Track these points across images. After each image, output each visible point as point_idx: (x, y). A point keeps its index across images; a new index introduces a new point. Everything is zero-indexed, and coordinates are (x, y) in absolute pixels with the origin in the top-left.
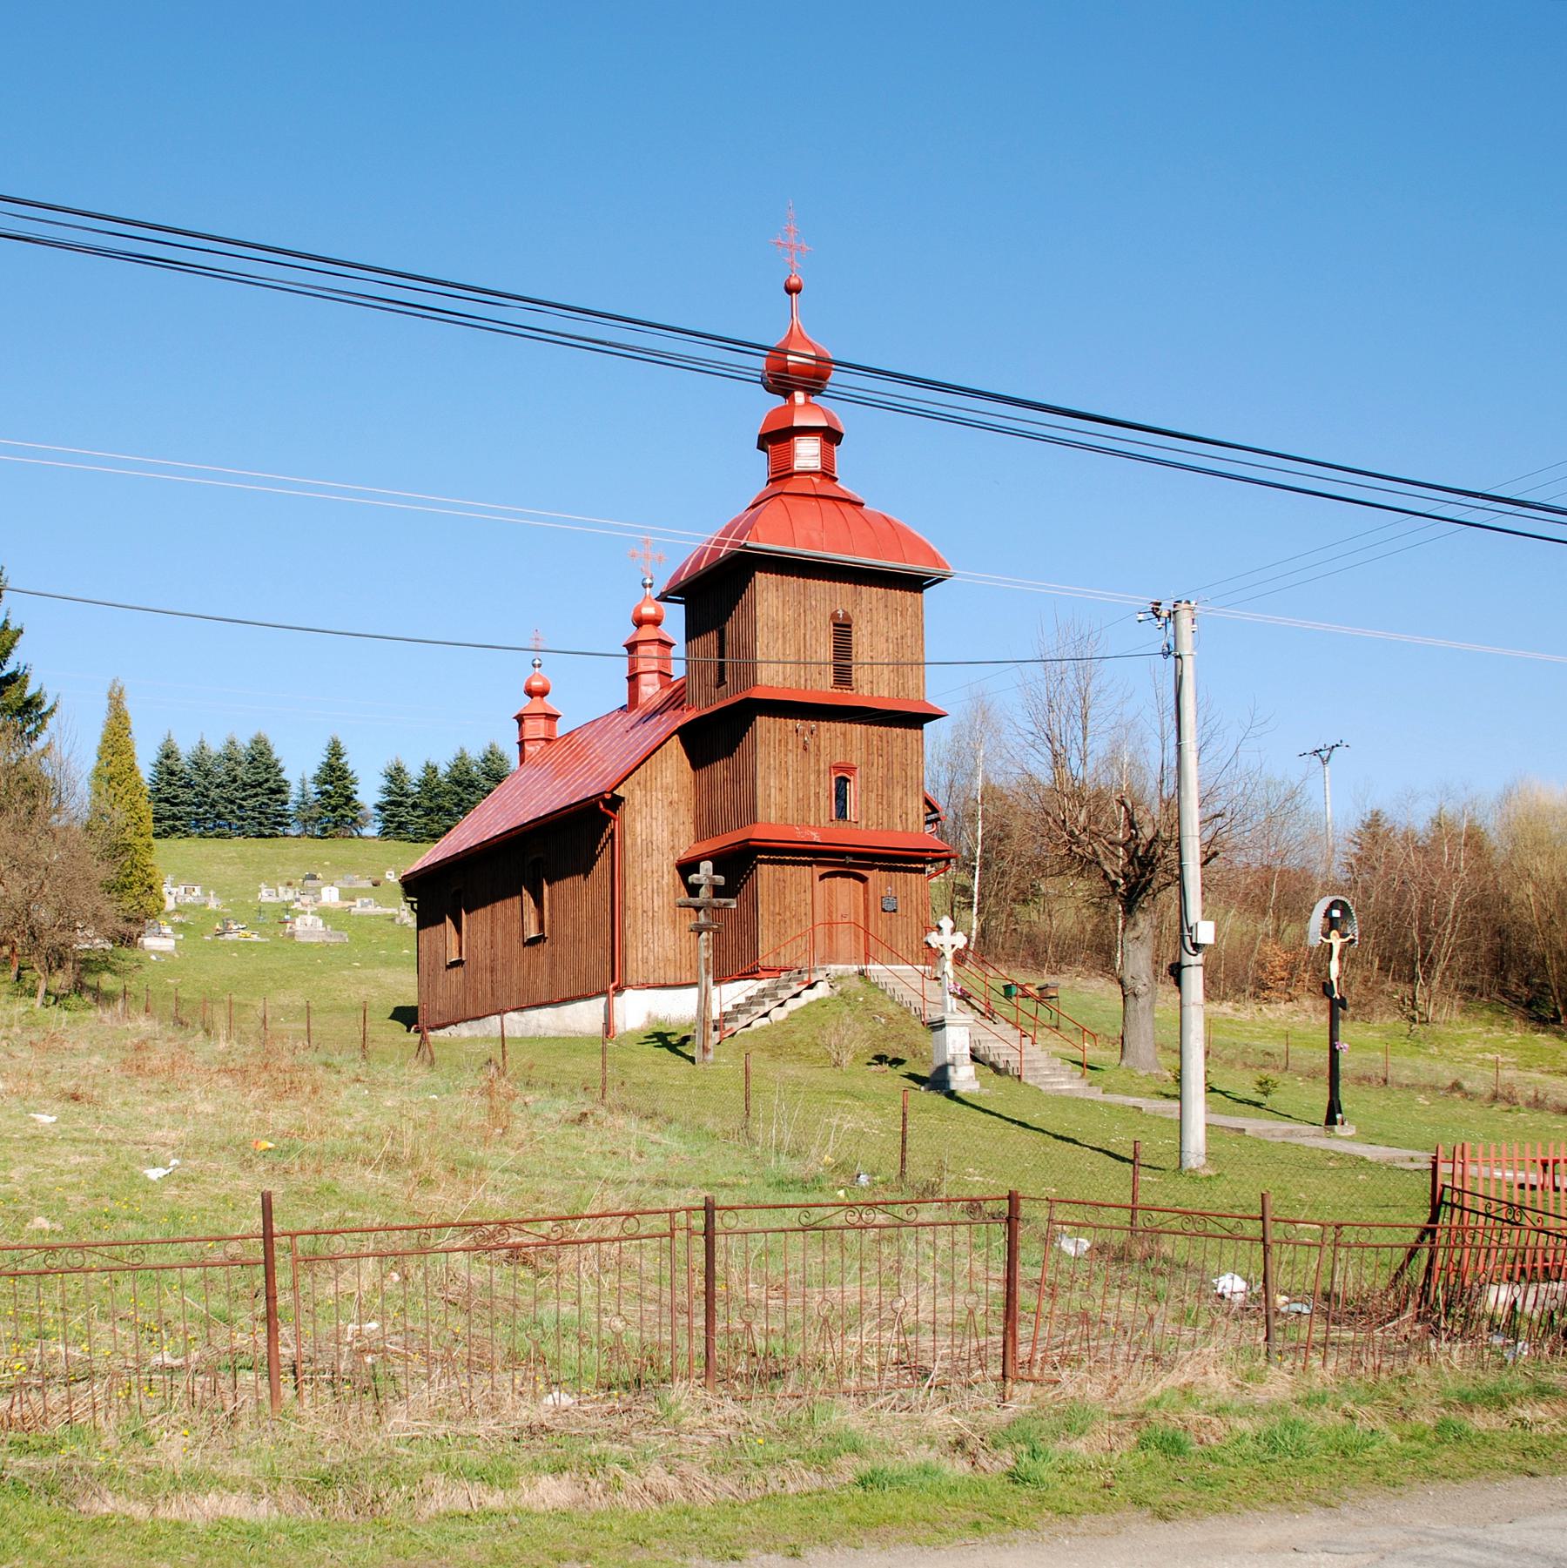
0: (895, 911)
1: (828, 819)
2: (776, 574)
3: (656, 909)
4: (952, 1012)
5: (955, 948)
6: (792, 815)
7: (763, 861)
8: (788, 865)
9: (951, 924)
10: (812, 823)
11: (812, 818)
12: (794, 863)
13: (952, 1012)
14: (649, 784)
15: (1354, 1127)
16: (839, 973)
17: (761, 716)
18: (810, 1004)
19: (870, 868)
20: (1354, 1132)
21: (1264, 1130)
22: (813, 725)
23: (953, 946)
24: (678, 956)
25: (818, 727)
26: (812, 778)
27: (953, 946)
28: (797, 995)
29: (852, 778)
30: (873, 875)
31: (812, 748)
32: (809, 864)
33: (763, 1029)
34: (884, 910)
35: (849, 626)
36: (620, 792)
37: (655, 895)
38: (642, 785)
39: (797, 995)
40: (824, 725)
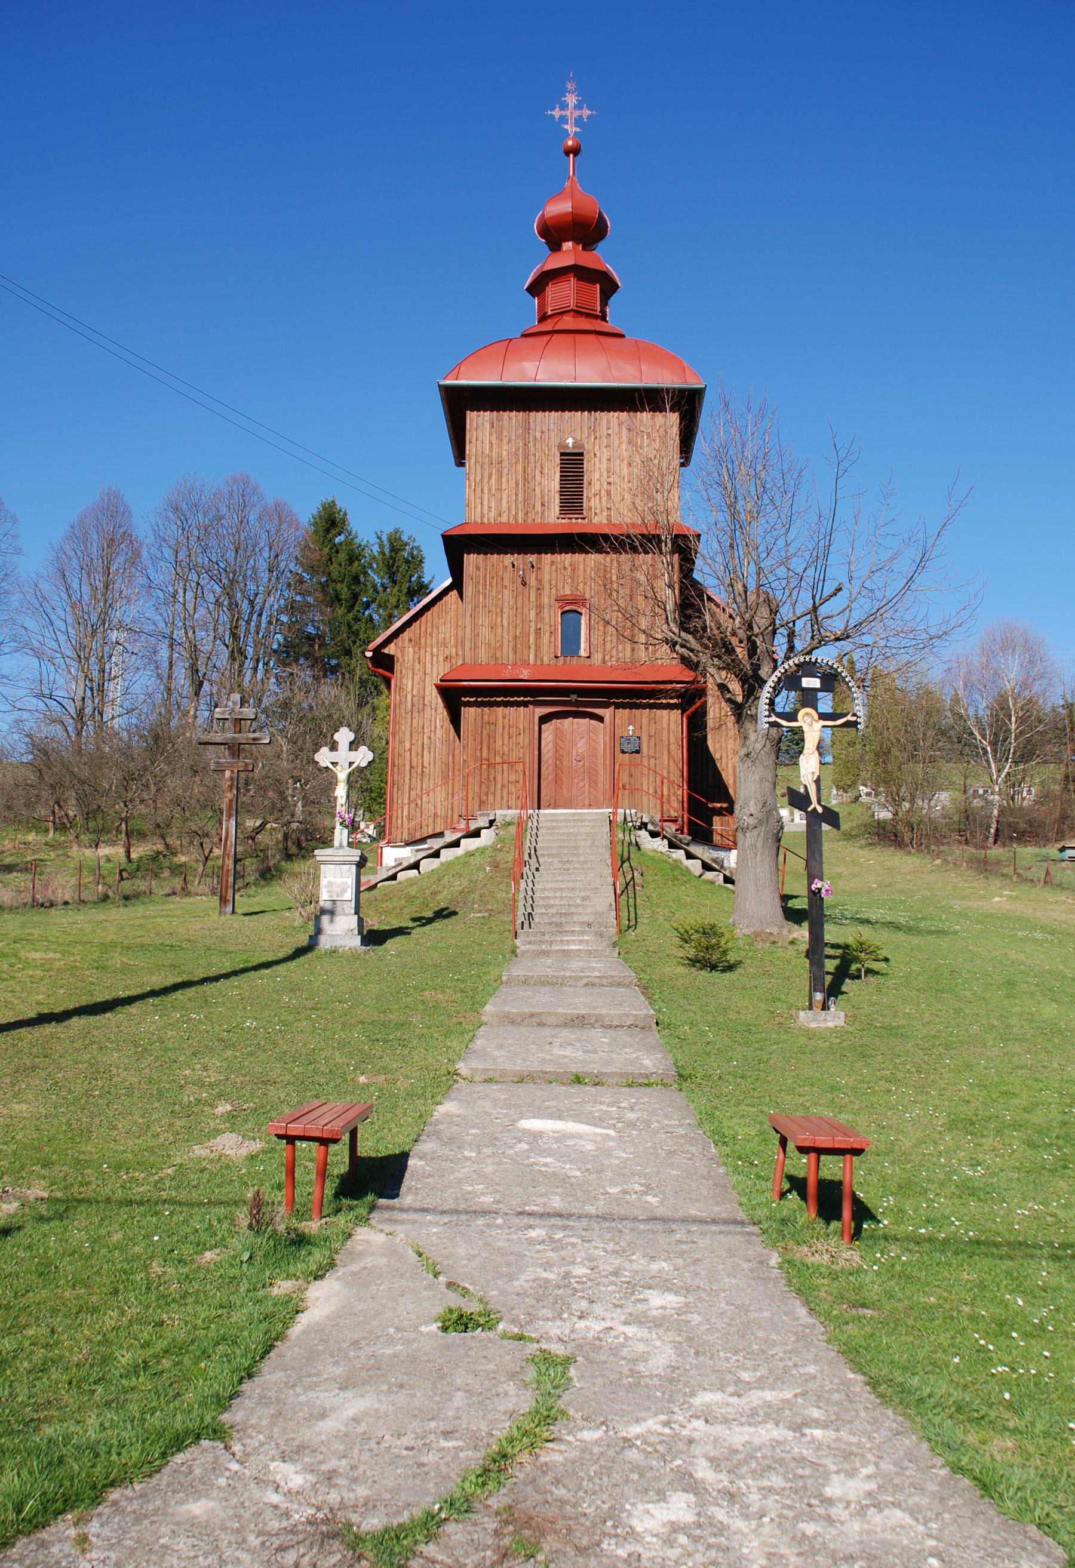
0: (637, 752)
1: (552, 655)
2: (492, 411)
3: (426, 764)
4: (341, 846)
5: (355, 766)
6: (507, 655)
7: (469, 704)
8: (499, 706)
9: (351, 736)
10: (532, 661)
11: (532, 657)
12: (507, 704)
13: (341, 846)
14: (423, 640)
15: (842, 1014)
16: (508, 819)
17: (469, 553)
18: (470, 854)
19: (606, 705)
20: (841, 1022)
21: (519, 1014)
22: (532, 558)
23: (351, 764)
24: (450, 812)
25: (539, 561)
26: (533, 614)
27: (351, 764)
28: (456, 844)
29: (583, 610)
30: (606, 713)
31: (532, 581)
32: (525, 704)
33: (411, 882)
34: (623, 752)
35: (582, 454)
36: (391, 650)
37: (426, 751)
38: (416, 642)
39: (456, 844)
40: (547, 558)
